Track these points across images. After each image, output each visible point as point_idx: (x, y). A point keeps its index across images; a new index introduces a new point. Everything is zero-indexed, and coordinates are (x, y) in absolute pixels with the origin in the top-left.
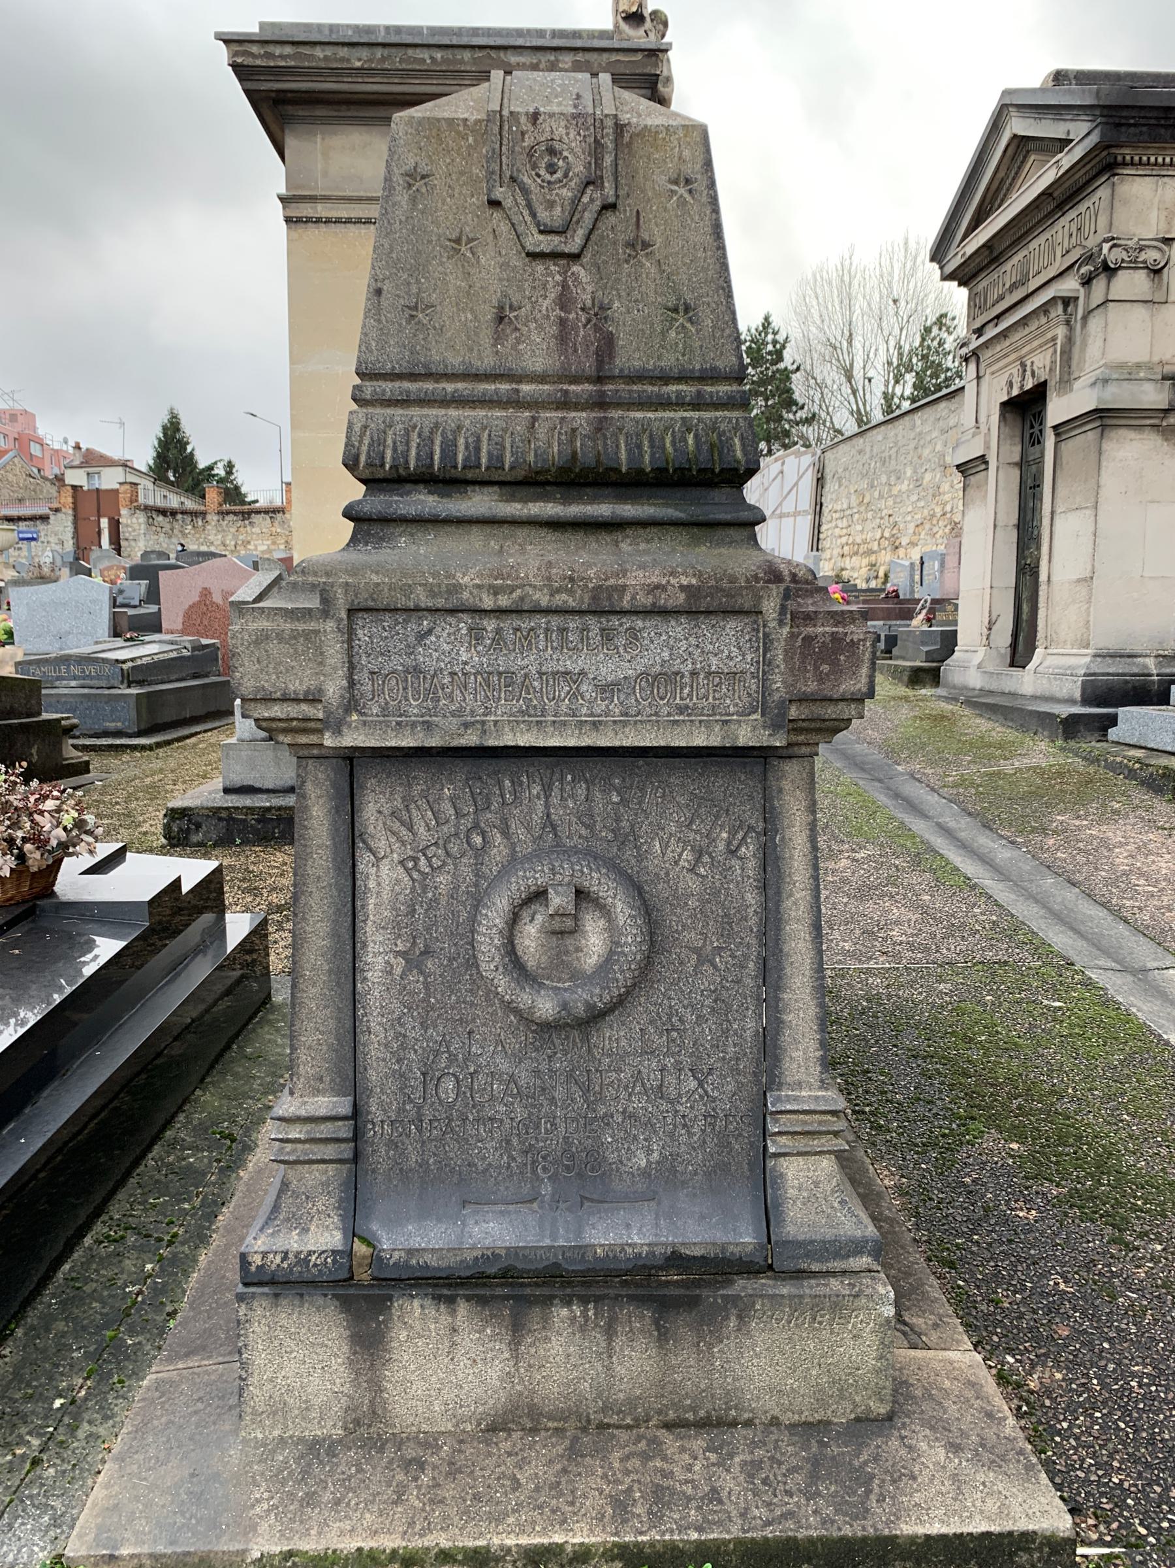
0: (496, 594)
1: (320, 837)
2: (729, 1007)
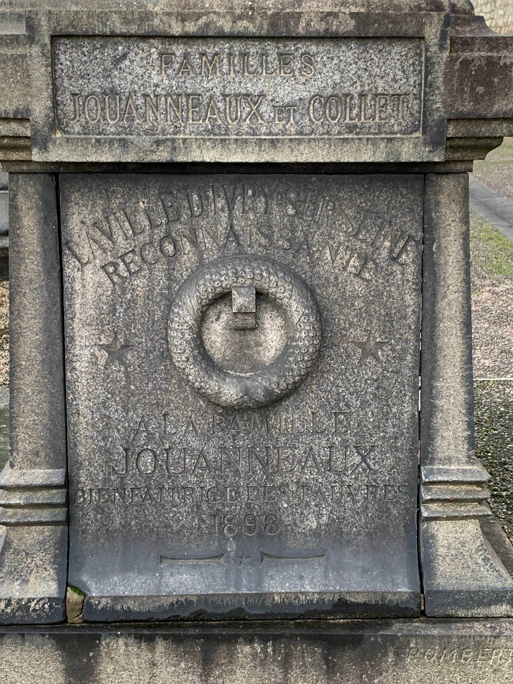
0: (183, 21)
1: (30, 244)
2: (389, 394)
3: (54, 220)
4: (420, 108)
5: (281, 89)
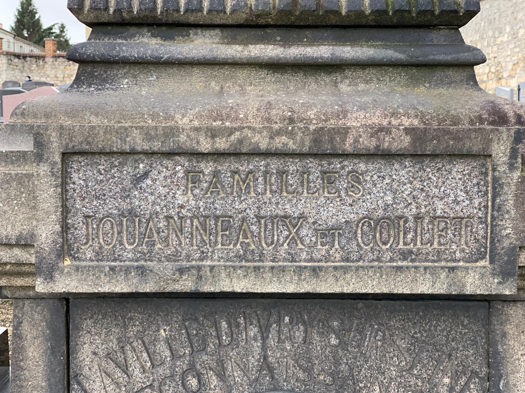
0: (213, 137)
1: (35, 378)
3: (62, 351)
4: (487, 233)
5: (324, 210)
